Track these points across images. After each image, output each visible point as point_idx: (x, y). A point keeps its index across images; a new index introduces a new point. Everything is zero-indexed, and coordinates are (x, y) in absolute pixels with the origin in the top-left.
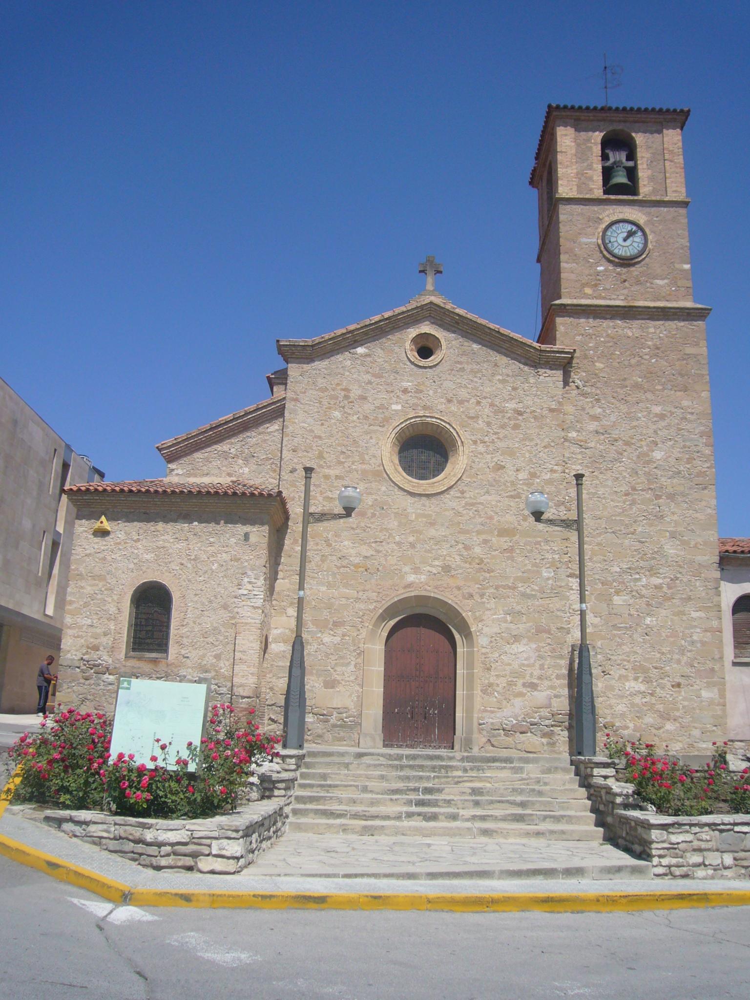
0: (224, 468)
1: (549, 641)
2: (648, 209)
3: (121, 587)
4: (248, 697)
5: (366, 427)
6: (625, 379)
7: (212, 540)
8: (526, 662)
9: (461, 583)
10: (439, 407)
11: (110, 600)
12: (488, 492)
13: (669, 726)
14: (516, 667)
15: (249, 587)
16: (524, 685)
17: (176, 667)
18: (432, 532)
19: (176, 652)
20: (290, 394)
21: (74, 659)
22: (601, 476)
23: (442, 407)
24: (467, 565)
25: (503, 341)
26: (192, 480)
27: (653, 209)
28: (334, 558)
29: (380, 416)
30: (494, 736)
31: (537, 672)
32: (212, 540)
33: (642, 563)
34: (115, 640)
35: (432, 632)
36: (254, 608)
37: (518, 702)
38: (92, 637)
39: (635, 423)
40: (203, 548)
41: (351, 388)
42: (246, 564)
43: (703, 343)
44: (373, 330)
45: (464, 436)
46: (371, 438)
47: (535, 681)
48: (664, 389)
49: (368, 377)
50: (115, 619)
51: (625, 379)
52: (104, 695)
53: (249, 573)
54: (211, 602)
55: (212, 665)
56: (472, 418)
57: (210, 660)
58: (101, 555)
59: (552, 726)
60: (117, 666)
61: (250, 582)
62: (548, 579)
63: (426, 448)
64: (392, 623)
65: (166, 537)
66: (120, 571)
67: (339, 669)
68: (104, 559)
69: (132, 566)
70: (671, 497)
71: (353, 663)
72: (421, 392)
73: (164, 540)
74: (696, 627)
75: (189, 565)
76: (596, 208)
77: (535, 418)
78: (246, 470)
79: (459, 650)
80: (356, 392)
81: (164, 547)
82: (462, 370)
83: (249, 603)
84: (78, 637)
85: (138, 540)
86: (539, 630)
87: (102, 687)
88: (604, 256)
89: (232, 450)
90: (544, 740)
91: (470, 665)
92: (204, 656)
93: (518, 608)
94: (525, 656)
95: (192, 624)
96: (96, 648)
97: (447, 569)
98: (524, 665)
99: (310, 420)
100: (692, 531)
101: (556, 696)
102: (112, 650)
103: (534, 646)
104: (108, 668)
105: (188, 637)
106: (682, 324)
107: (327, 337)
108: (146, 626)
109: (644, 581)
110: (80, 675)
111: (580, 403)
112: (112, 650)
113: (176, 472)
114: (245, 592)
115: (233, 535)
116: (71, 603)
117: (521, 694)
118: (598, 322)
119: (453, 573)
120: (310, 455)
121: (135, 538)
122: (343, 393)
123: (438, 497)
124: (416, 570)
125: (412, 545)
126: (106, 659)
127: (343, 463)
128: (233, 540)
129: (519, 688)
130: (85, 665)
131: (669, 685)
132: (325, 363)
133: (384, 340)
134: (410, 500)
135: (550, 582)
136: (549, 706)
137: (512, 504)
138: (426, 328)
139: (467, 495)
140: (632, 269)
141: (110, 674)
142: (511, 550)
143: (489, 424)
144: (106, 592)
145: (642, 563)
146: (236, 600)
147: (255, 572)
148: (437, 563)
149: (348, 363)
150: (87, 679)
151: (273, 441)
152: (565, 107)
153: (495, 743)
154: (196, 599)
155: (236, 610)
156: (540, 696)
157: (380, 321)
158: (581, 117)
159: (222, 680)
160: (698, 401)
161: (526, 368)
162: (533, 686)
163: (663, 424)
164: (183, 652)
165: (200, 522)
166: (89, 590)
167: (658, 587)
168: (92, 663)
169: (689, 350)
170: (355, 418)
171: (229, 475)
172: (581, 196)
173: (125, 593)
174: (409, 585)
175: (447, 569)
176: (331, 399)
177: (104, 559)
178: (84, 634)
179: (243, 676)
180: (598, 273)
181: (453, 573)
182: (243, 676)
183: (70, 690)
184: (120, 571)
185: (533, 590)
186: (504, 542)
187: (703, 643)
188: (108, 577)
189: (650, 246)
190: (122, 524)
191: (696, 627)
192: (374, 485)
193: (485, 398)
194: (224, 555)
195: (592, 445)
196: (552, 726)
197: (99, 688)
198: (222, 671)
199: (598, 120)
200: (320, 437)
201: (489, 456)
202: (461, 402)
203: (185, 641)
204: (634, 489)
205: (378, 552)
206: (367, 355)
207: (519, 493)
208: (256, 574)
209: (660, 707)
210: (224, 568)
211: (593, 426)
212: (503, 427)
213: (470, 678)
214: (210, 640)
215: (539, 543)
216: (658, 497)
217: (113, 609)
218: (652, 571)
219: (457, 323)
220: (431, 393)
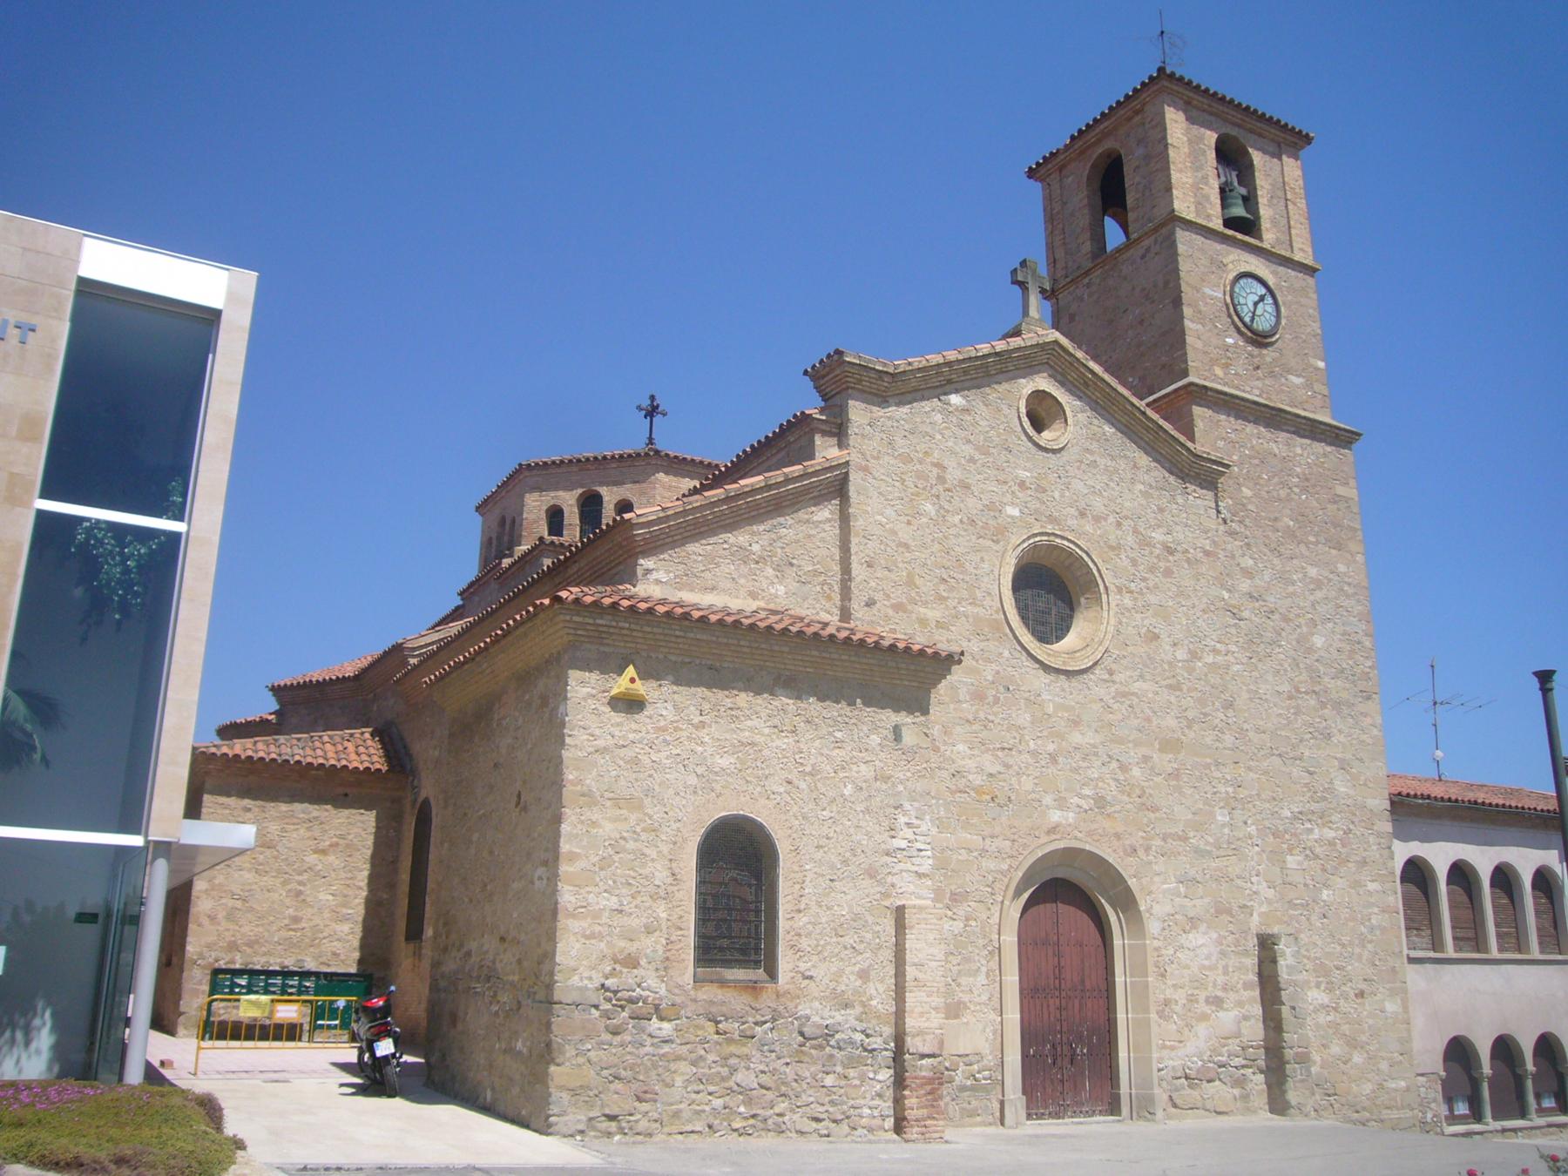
0: (742, 581)
1: (1231, 927)
2: (1274, 267)
3: (675, 826)
4: (929, 1056)
5: (974, 538)
6: (1276, 519)
7: (839, 735)
8: (1206, 963)
9: (1120, 829)
10: (1069, 522)
11: (652, 853)
12: (1141, 676)
13: (1357, 1058)
14: (1196, 970)
15: (909, 833)
16: (1207, 1001)
17: (792, 999)
18: (1076, 738)
19: (791, 966)
20: (854, 457)
21: (586, 988)
22: (1260, 665)
23: (1072, 522)
24: (1125, 798)
25: (1147, 429)
26: (689, 597)
27: (1281, 269)
28: (945, 774)
29: (991, 522)
30: (1177, 1090)
31: (1221, 979)
32: (839, 735)
33: (1314, 806)
34: (669, 942)
35: (1072, 909)
36: (919, 875)
37: (1202, 1029)
38: (622, 936)
39: (1291, 589)
40: (825, 751)
41: (945, 463)
42: (901, 788)
43: (1353, 483)
44: (976, 368)
45: (1108, 571)
46: (982, 560)
47: (1220, 994)
48: (1317, 543)
49: (968, 450)
50: (667, 897)
51: (1276, 519)
52: (655, 1066)
53: (907, 806)
54: (845, 862)
55: (856, 992)
56: (1112, 548)
57: (850, 982)
58: (629, 753)
59: (1243, 1067)
60: (678, 1000)
61: (908, 824)
62: (1223, 826)
63: (1051, 588)
64: (1026, 895)
65: (755, 722)
66: (671, 791)
67: (964, 981)
68: (635, 761)
69: (693, 780)
70: (1337, 705)
71: (984, 969)
72: (1044, 491)
73: (751, 729)
74: (1373, 905)
75: (803, 785)
76: (1219, 247)
77: (1188, 561)
78: (781, 590)
79: (1117, 942)
80: (953, 474)
81: (752, 744)
82: (1094, 464)
83: (909, 866)
84: (592, 936)
85: (702, 725)
86: (1221, 910)
87: (648, 1049)
88: (1233, 322)
89: (755, 548)
90: (1236, 1091)
91: (1139, 969)
92: (841, 972)
93: (1192, 873)
94: (1205, 951)
95: (814, 908)
96: (632, 962)
97: (1100, 802)
98: (1204, 967)
99: (889, 512)
100: (1361, 760)
101: (1246, 1018)
102: (666, 965)
103: (1215, 936)
104: (657, 1008)
105: (809, 935)
106: (1329, 449)
107: (916, 365)
108: (715, 909)
109: (1316, 834)
110: (602, 1024)
111: (1229, 547)
112: (666, 965)
113: (655, 575)
114: (904, 844)
115: (875, 729)
116: (573, 857)
117: (1204, 1017)
118: (1239, 424)
119: (1110, 810)
120: (893, 576)
121: (696, 721)
122: (935, 471)
123: (1080, 678)
124: (1062, 804)
125: (1053, 758)
126: (653, 986)
127: (946, 599)
128: (875, 739)
129: (1202, 1007)
130: (610, 1000)
131: (1352, 994)
132: (905, 409)
133: (987, 390)
134: (1045, 678)
135: (1226, 831)
136: (1238, 1035)
137: (1173, 699)
138: (1043, 383)
139: (1117, 678)
140: (1265, 352)
141: (661, 1019)
142: (1175, 775)
143: (1134, 562)
144: (644, 836)
145: (1314, 806)
146: (889, 859)
147: (916, 804)
148: (1086, 791)
149: (938, 417)
150: (615, 1033)
151: (823, 540)
152: (1181, 79)
153: (1178, 1102)
154: (819, 855)
155: (889, 879)
156: (1227, 1018)
157: (989, 355)
158: (1205, 103)
159: (874, 1022)
160: (1351, 567)
161: (1172, 479)
162: (1217, 1002)
163: (1319, 595)
164: (803, 966)
165: (821, 699)
166: (608, 829)
167: (1331, 843)
168: (626, 994)
169: (1341, 490)
170: (957, 519)
171: (753, 595)
172: (1199, 221)
173: (685, 840)
174: (1053, 830)
175: (1100, 802)
176: (919, 478)
177: (635, 761)
178: (605, 930)
179: (922, 1014)
180: (1227, 348)
181: (1110, 810)
182: (922, 1014)
183: (581, 1060)
184: (671, 791)
185: (1207, 843)
186: (1164, 761)
187: (1383, 930)
188: (647, 801)
189: (1283, 322)
190: (668, 688)
191: (1373, 905)
192: (992, 645)
193: (1126, 518)
194: (863, 767)
195: (1246, 614)
196: (1243, 1067)
197: (643, 1051)
198: (874, 1003)
199: (1211, 114)
200: (906, 546)
201: (1138, 616)
202: (1097, 519)
203: (804, 943)
204: (1298, 691)
205: (1008, 766)
206: (966, 410)
207: (1179, 682)
208: (918, 809)
209: (1346, 1028)
210: (865, 794)
211: (1245, 585)
212: (1152, 570)
213: (1142, 991)
214: (849, 940)
215: (1207, 766)
216: (1323, 705)
217: (662, 876)
218: (1323, 818)
219: (1086, 385)
220: (1057, 495)
